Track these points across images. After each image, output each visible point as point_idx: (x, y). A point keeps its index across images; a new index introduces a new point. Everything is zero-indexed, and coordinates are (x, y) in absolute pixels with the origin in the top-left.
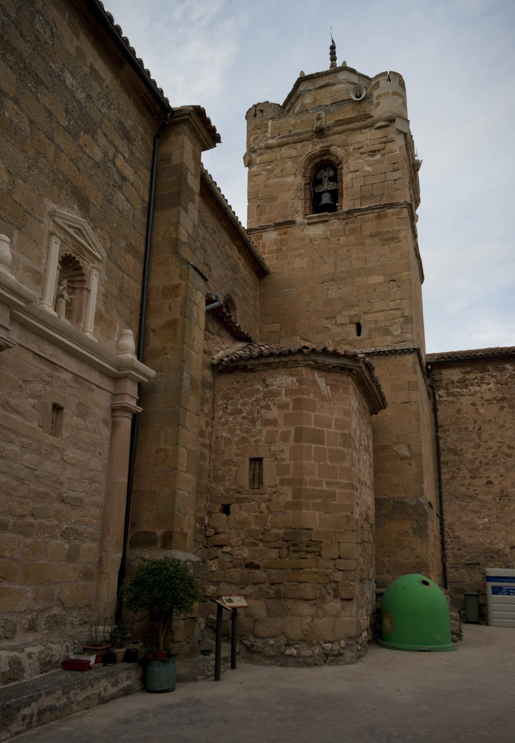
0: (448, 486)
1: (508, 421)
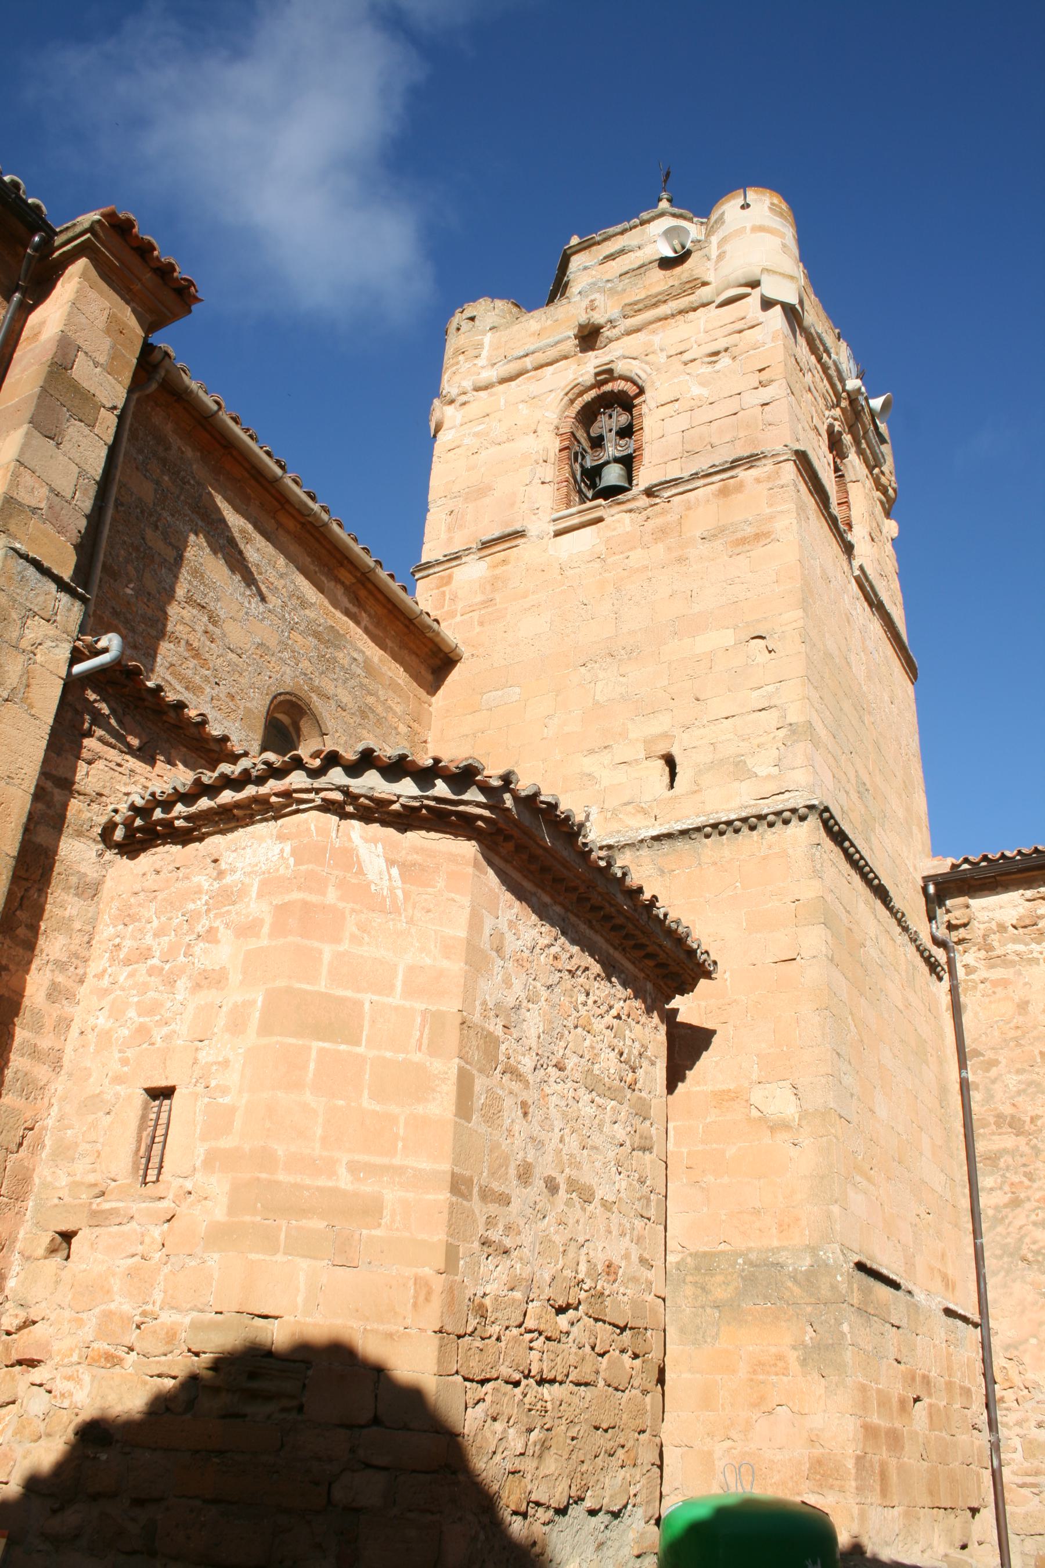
0: (1000, 1229)
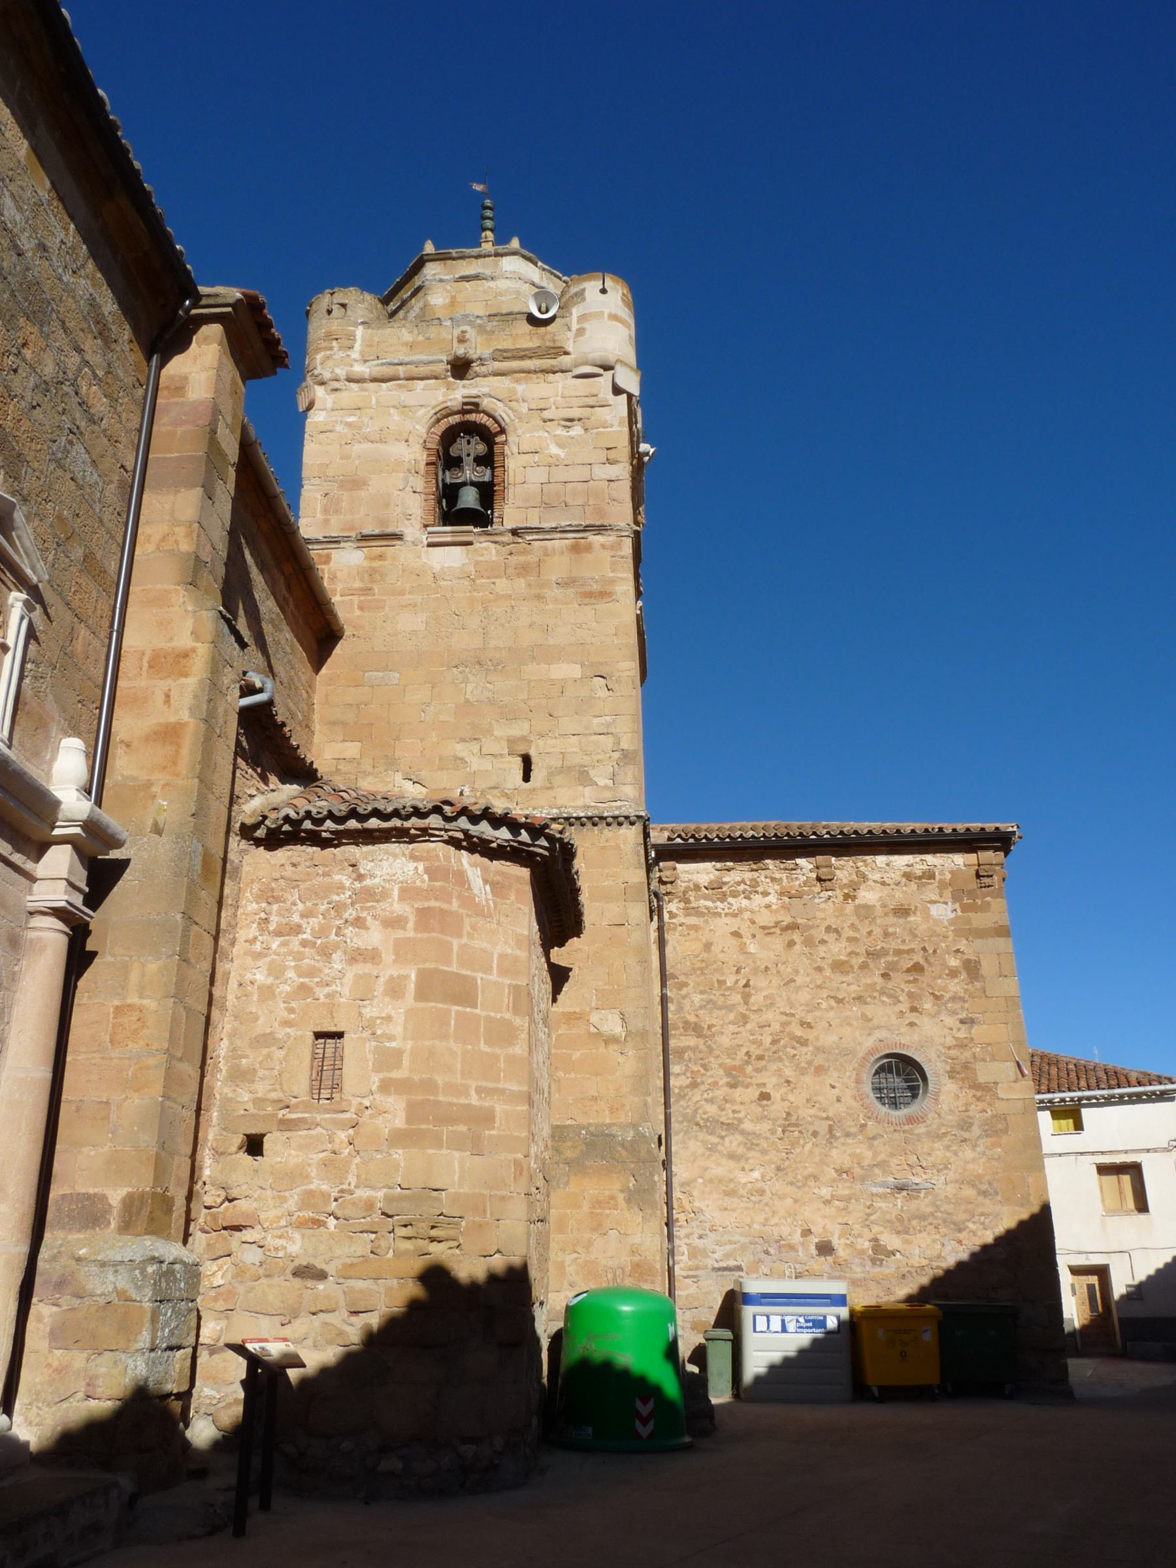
0: (682, 1103)
1: (802, 971)
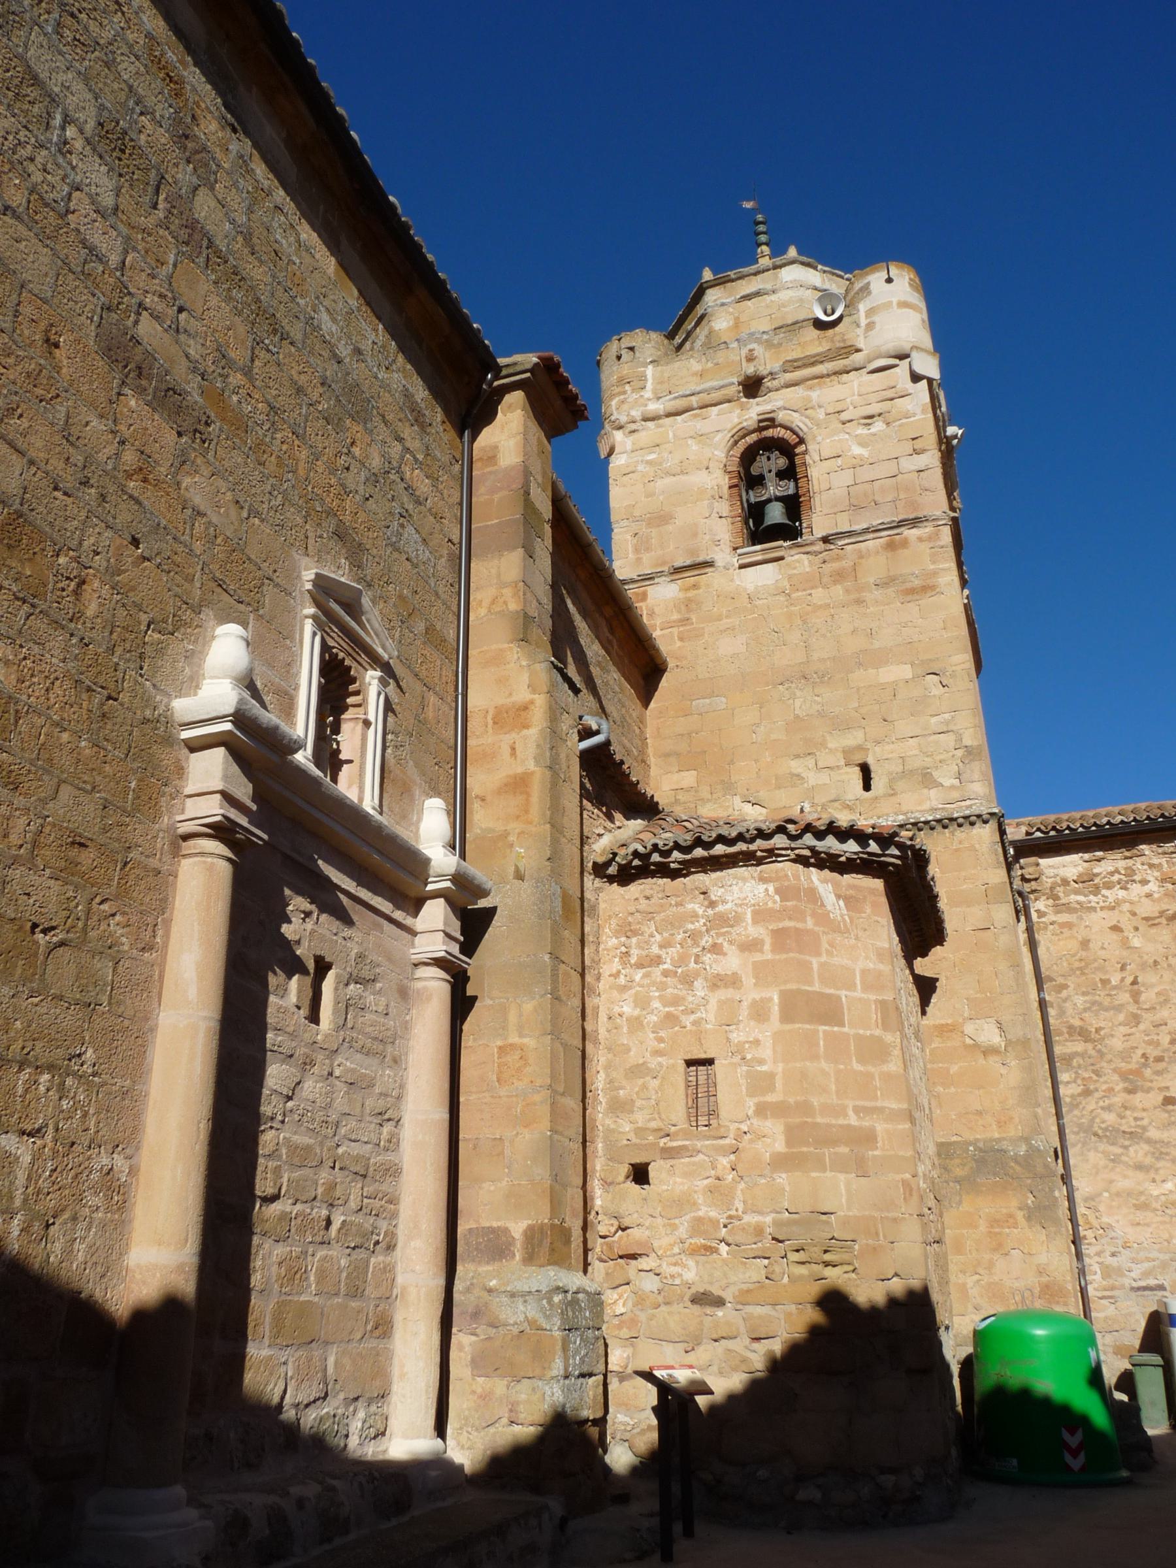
0: (1076, 1112)
